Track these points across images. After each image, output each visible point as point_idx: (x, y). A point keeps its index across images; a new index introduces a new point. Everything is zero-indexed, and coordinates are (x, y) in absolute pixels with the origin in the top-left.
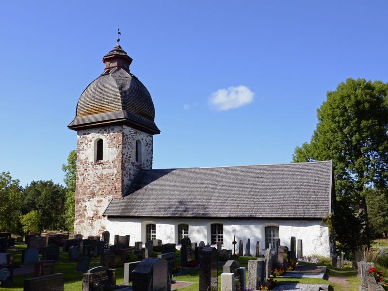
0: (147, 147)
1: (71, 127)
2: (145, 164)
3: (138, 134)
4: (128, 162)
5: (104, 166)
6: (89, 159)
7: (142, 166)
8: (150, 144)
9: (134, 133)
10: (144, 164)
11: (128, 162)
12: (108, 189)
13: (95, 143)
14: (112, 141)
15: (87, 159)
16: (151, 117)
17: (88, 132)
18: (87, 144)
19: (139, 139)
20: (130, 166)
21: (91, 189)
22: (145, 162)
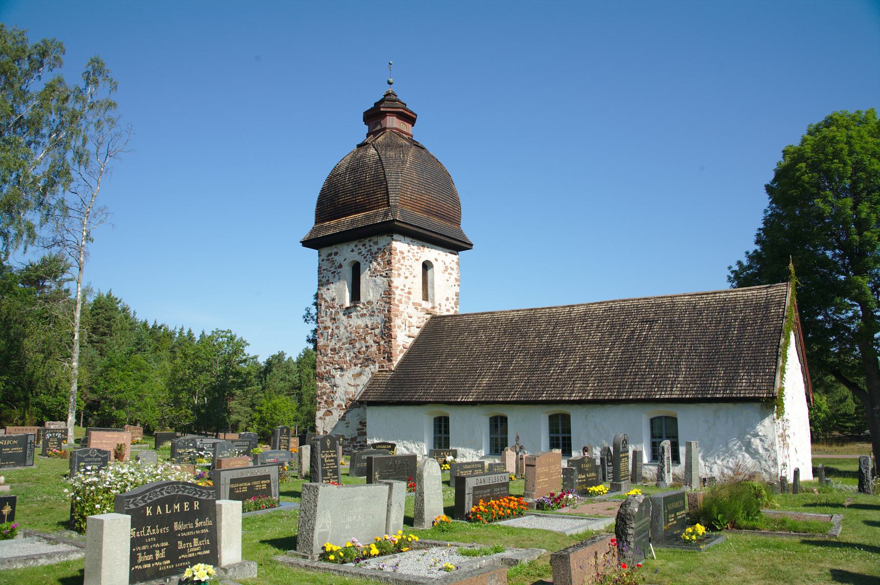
0: (446, 274)
1: (307, 243)
2: (443, 305)
4: (407, 303)
10: (440, 305)
11: (407, 303)
16: (454, 218)
17: (335, 250)
22: (443, 303)
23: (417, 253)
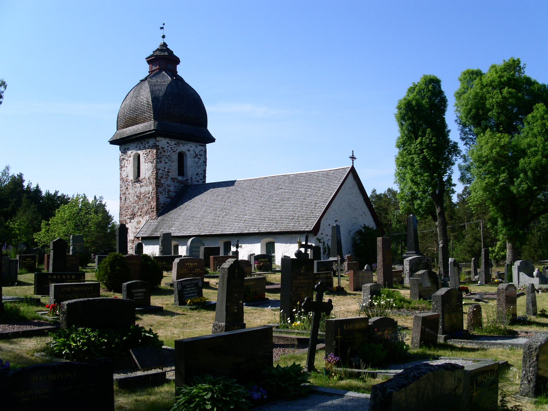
1: (112, 142)
2: (194, 178)
3: (181, 145)
5: (141, 184)
6: (129, 176)
7: (189, 181)
8: (201, 155)
9: (175, 144)
10: (191, 178)
12: (146, 208)
13: (134, 159)
14: (147, 156)
15: (127, 176)
18: (128, 160)
19: (184, 150)
20: (169, 182)
21: (131, 210)
23: (175, 147)
